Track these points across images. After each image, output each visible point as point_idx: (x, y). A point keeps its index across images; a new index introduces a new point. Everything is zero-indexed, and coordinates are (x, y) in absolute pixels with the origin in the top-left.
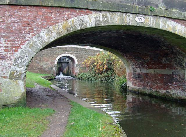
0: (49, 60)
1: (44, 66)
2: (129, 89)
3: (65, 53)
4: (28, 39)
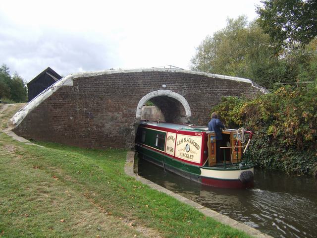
0: (118, 109)
1: (108, 126)
2: (169, 134)
3: (160, 87)
4: (295, 139)
